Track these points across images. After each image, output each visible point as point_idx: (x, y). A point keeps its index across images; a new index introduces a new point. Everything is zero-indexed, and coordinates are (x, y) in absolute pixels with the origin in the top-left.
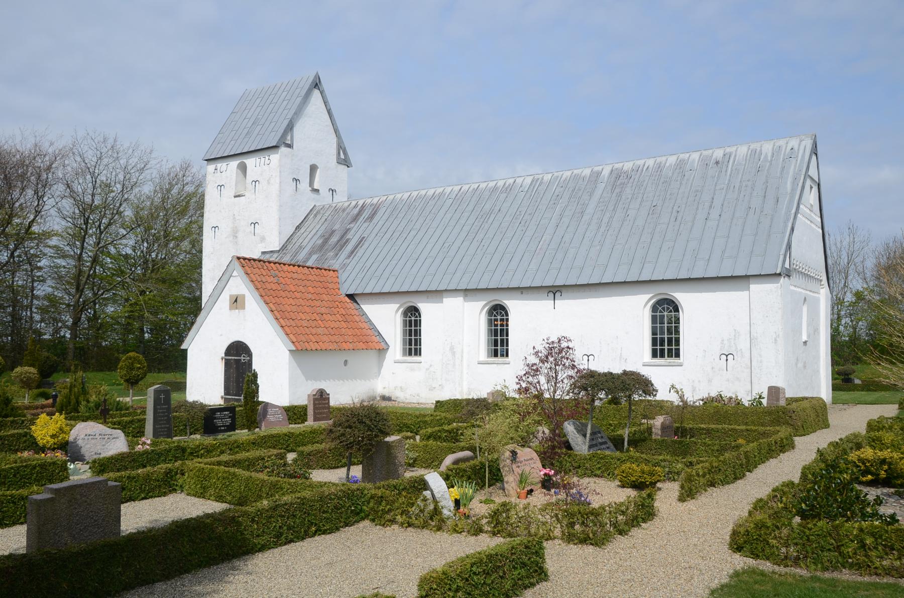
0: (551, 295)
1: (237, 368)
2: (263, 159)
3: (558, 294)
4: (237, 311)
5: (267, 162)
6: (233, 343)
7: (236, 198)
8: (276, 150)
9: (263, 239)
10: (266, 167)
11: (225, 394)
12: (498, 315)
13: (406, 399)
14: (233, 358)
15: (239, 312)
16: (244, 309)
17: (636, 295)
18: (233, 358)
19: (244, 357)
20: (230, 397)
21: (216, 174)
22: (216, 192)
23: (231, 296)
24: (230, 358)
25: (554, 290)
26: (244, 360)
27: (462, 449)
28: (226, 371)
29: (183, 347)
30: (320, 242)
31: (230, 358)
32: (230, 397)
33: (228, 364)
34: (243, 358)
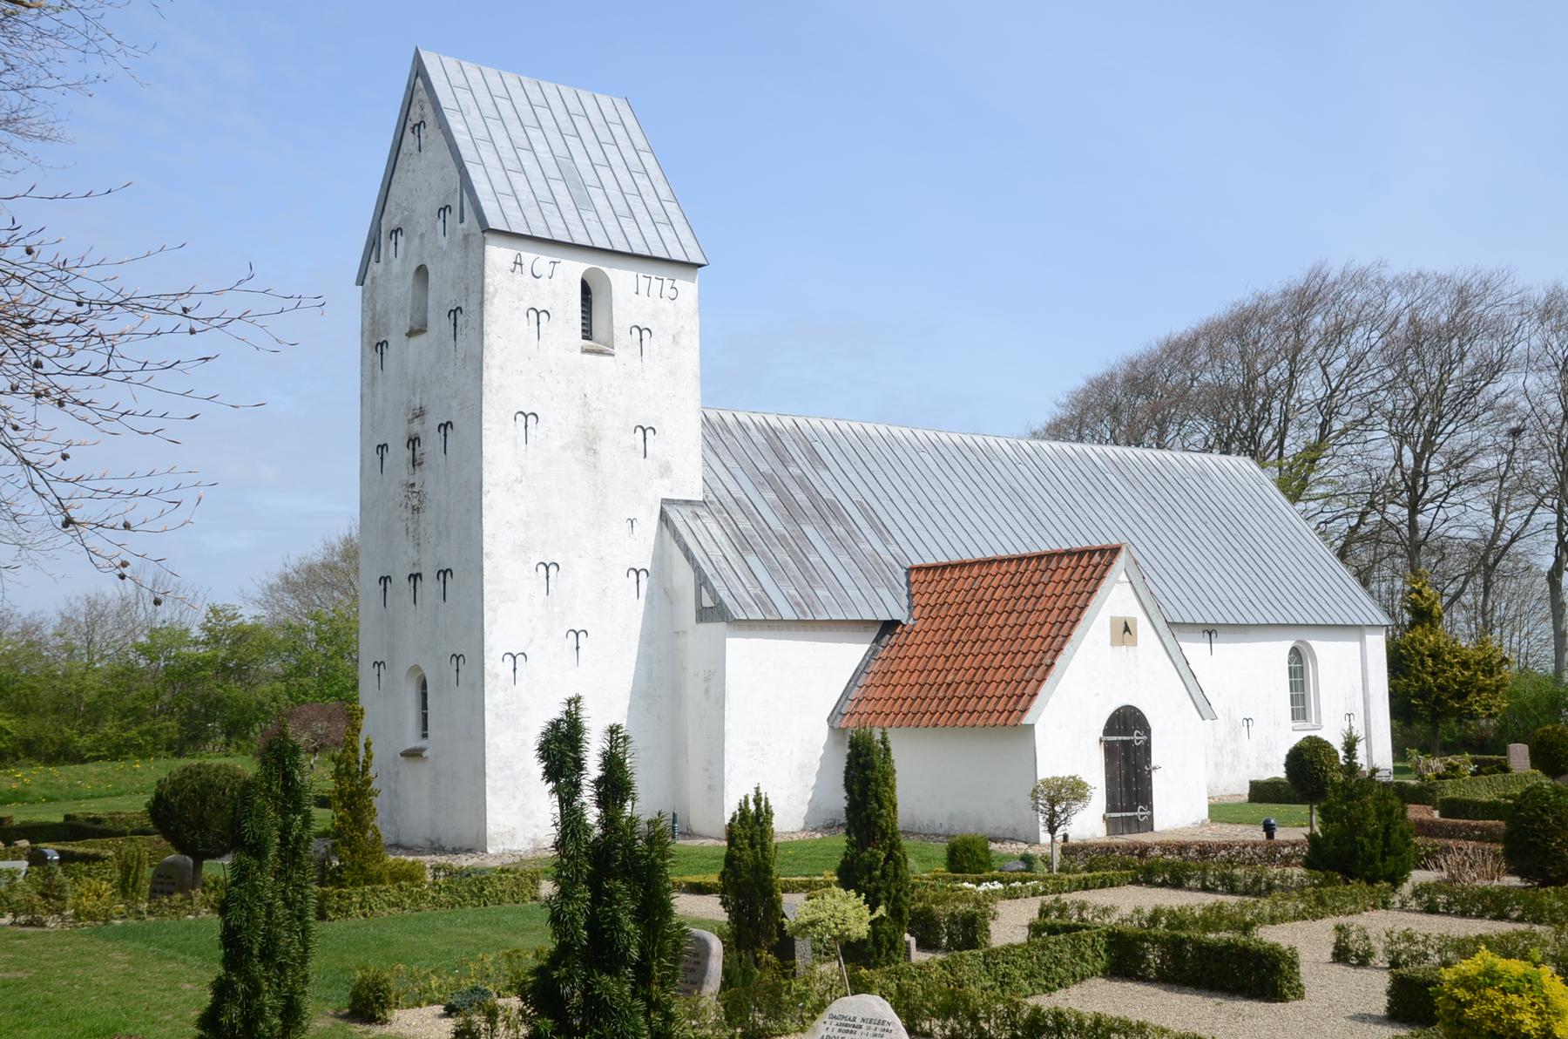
0: (1207, 635)
1: (1127, 759)
2: (656, 284)
3: (1213, 635)
4: (1124, 648)
5: (668, 292)
6: (1118, 710)
7: (587, 356)
8: (689, 271)
9: (665, 470)
10: (665, 303)
11: (1109, 810)
12: (1298, 662)
13: (556, 825)
14: (1120, 738)
15: (1127, 651)
16: (1136, 645)
17: (1337, 641)
18: (1120, 738)
19: (1138, 735)
20: (1118, 815)
21: (517, 275)
22: (527, 327)
23: (1114, 620)
24: (1115, 738)
25: (1210, 629)
26: (1138, 741)
27: (992, 880)
28: (1107, 765)
29: (1027, 720)
30: (771, 496)
31: (1115, 738)
32: (1118, 815)
33: (1110, 750)
34: (1137, 738)
